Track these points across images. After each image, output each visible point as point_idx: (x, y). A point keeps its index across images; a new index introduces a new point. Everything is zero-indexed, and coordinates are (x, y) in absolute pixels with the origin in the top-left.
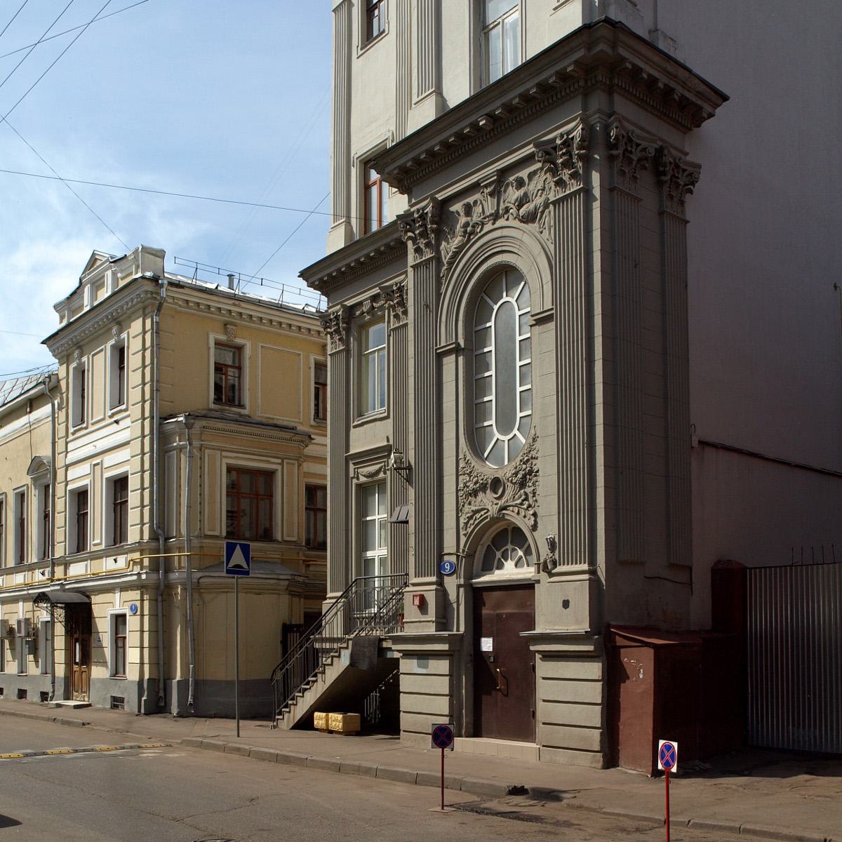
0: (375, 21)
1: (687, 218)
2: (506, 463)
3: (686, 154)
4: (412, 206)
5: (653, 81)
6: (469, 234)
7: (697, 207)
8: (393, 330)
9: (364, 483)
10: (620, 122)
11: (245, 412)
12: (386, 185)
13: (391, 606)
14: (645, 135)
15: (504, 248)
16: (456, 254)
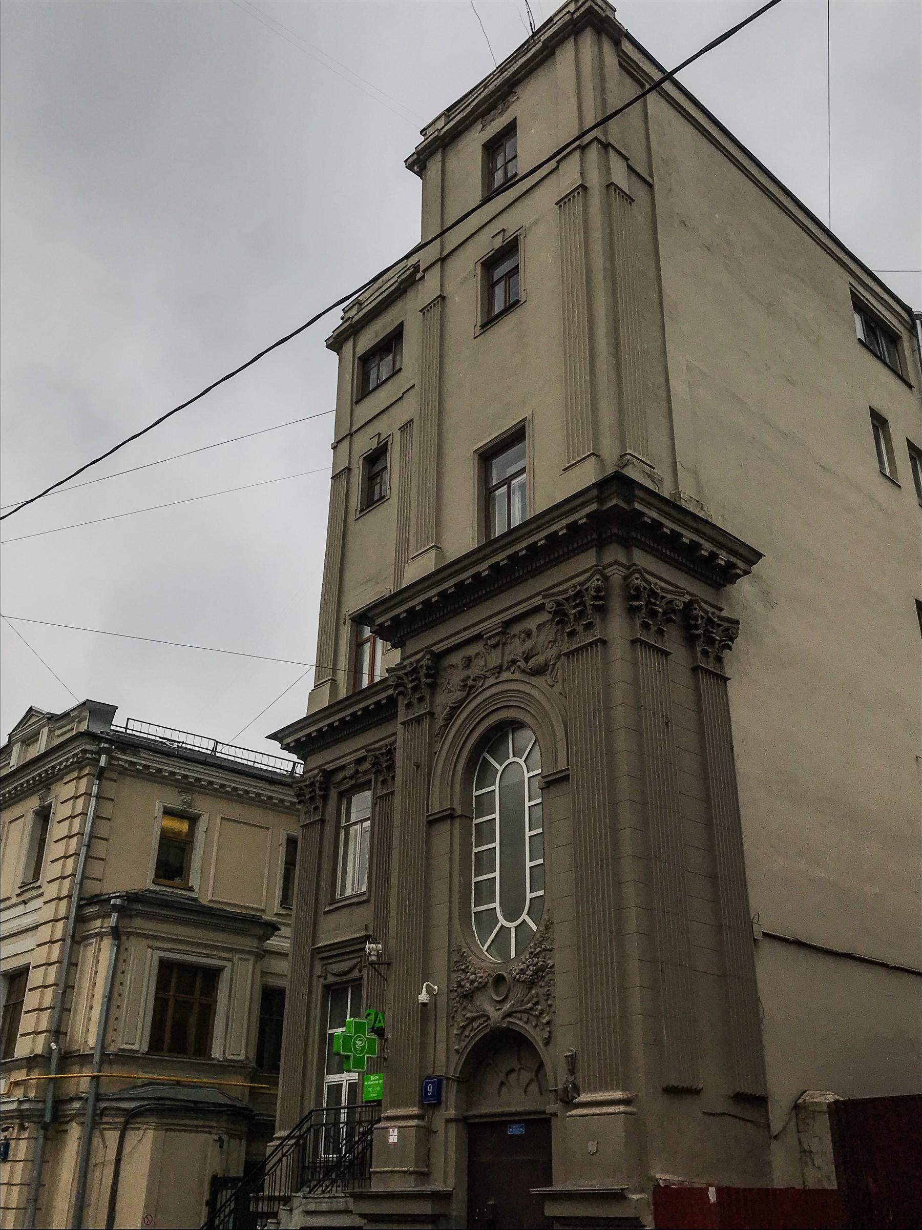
0: (377, 488)
2: (513, 956)
3: (721, 609)
6: (469, 688)
8: (380, 797)
9: (337, 983)
10: (640, 573)
11: (193, 895)
12: (380, 642)
14: (670, 588)
15: (511, 703)
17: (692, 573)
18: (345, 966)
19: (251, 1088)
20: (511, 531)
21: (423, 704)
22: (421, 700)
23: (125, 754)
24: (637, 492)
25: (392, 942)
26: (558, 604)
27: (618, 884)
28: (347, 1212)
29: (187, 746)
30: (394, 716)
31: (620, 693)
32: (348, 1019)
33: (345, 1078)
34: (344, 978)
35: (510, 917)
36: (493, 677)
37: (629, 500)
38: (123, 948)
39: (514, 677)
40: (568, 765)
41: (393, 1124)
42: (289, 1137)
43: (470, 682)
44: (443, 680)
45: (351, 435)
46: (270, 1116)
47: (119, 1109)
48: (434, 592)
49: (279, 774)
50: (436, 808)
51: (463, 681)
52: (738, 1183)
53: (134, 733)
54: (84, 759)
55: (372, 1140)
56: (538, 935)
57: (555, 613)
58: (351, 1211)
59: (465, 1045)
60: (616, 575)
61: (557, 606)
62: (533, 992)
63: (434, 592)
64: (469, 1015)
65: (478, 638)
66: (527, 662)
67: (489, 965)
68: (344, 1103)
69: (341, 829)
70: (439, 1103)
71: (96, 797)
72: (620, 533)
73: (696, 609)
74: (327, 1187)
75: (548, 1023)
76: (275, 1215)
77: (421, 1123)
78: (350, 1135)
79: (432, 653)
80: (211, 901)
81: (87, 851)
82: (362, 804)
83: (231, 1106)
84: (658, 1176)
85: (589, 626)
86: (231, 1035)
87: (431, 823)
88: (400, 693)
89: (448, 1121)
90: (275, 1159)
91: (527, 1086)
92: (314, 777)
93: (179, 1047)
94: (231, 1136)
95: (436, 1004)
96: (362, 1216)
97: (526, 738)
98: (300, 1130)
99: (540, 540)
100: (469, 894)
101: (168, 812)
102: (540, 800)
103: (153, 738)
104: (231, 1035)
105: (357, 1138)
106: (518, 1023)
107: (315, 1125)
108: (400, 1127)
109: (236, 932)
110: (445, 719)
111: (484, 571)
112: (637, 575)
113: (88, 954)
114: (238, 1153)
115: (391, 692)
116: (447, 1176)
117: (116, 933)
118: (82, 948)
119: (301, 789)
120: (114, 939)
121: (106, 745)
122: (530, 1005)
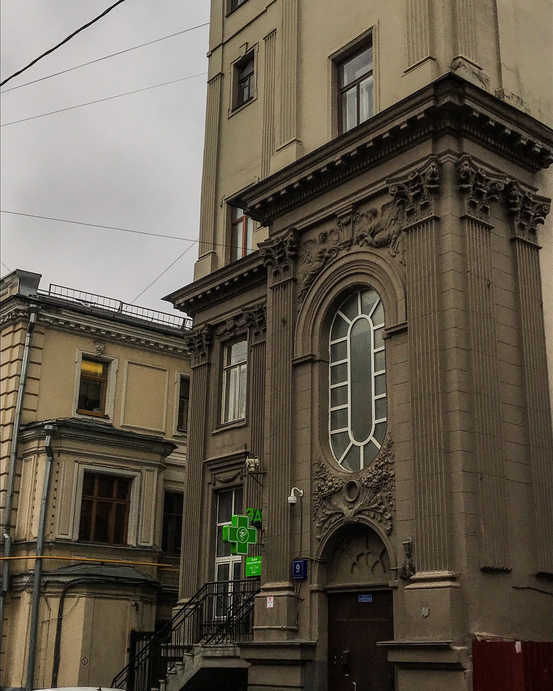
0: (246, 91)
1: (540, 245)
2: (362, 468)
6: (325, 259)
8: (254, 346)
9: (221, 489)
10: (469, 160)
11: (109, 422)
12: (251, 222)
13: (241, 615)
16: (313, 276)
17: (512, 159)
18: (230, 475)
19: (159, 567)
20: (360, 127)
22: (286, 268)
23: (49, 313)
24: (467, 90)
25: (267, 458)
26: (400, 188)
27: (446, 411)
28: (235, 657)
29: (99, 306)
30: (265, 281)
31: (451, 261)
32: (233, 515)
33: (232, 560)
34: (227, 485)
35: (359, 438)
36: (345, 250)
37: (461, 97)
38: (55, 463)
39: (364, 249)
40: (407, 320)
41: (270, 593)
42: (189, 603)
43: (326, 254)
44: (303, 253)
45: (223, 44)
46: (175, 588)
47: (58, 582)
48: (295, 180)
49: (172, 328)
50: (299, 354)
51: (320, 253)
52: (537, 638)
53: (56, 296)
54: (18, 317)
55: (253, 605)
57: (398, 195)
58: (239, 657)
60: (448, 162)
61: (399, 190)
62: (378, 495)
63: (295, 180)
65: (333, 217)
66: (373, 237)
67: (343, 474)
68: (231, 578)
69: (224, 370)
70: (305, 578)
71: (29, 346)
72: (453, 126)
73: (515, 190)
74: (219, 640)
75: (390, 519)
76: (181, 659)
77: (293, 593)
78: (236, 601)
79: (295, 230)
80: (122, 426)
81: (24, 389)
82: (240, 351)
83: (143, 580)
84: (477, 633)
85: (425, 206)
86: (142, 526)
87: (296, 366)
89: (312, 592)
90: (179, 620)
91: (373, 567)
92: (201, 330)
93: (101, 536)
94: (145, 602)
95: (301, 503)
96: (247, 660)
97: (372, 298)
98: (198, 598)
99: (385, 134)
100: (326, 419)
101: (86, 358)
102: (383, 348)
103: (71, 299)
104: (142, 526)
105: (242, 605)
106: (368, 519)
107: (209, 594)
108: (275, 596)
109: (145, 450)
110: (306, 284)
111: (338, 160)
112: (466, 162)
113: (28, 467)
114: (150, 613)
115: (261, 262)
116: (312, 631)
117: (49, 451)
118: (23, 462)
119: (191, 340)
120: (48, 456)
121: (35, 306)
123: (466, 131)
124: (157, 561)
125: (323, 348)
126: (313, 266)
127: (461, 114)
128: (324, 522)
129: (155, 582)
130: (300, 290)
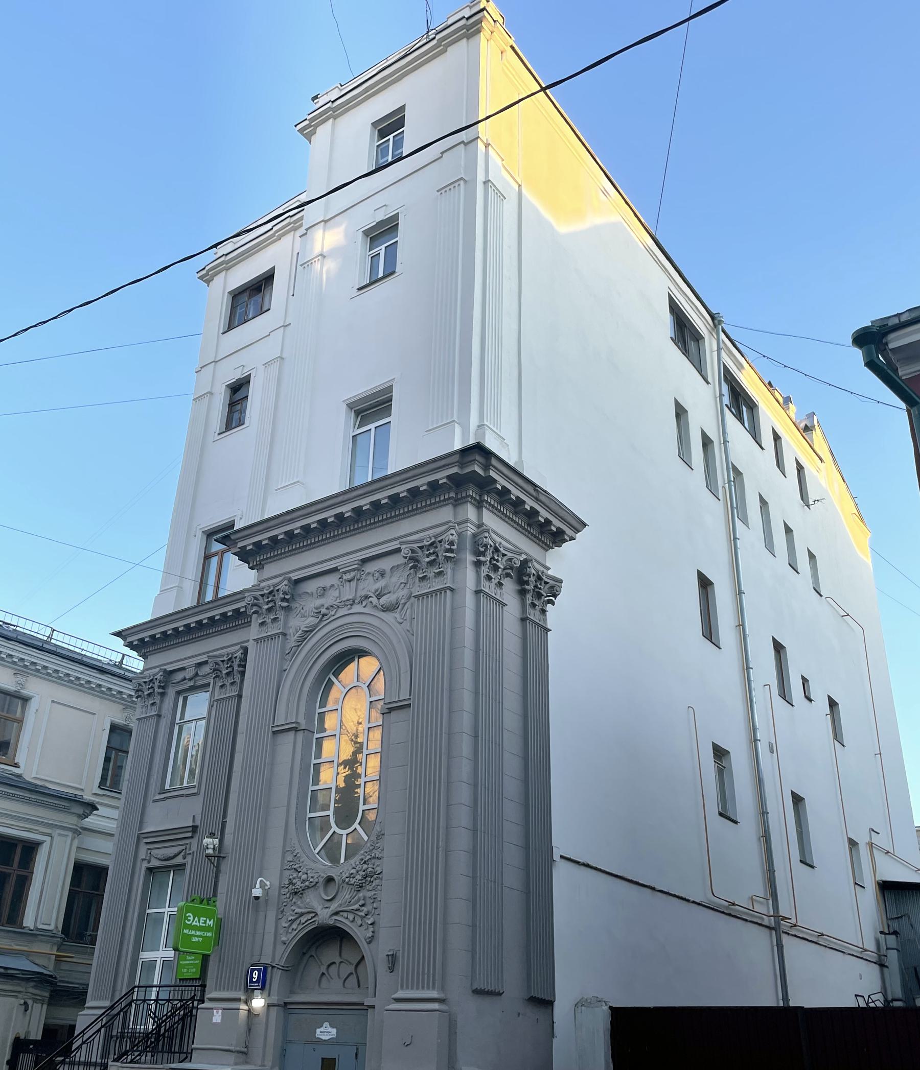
1: (549, 627)
2: (342, 861)
3: (548, 569)
4: (261, 581)
5: (534, 513)
7: (555, 615)
14: (510, 547)
19: (57, 956)
21: (276, 625)
22: (275, 620)
25: (228, 837)
36: (346, 608)
43: (324, 611)
44: (298, 605)
50: (280, 720)
56: (369, 845)
59: (292, 936)
64: (297, 910)
65: (335, 570)
79: (289, 580)
83: (38, 973)
88: (255, 612)
94: (35, 1001)
97: (368, 666)
122: (357, 906)
123: (487, 502)
124: (55, 948)
125: (309, 716)
126: (307, 622)
127: (485, 484)
128: (293, 921)
129: (51, 976)
130: (288, 646)
